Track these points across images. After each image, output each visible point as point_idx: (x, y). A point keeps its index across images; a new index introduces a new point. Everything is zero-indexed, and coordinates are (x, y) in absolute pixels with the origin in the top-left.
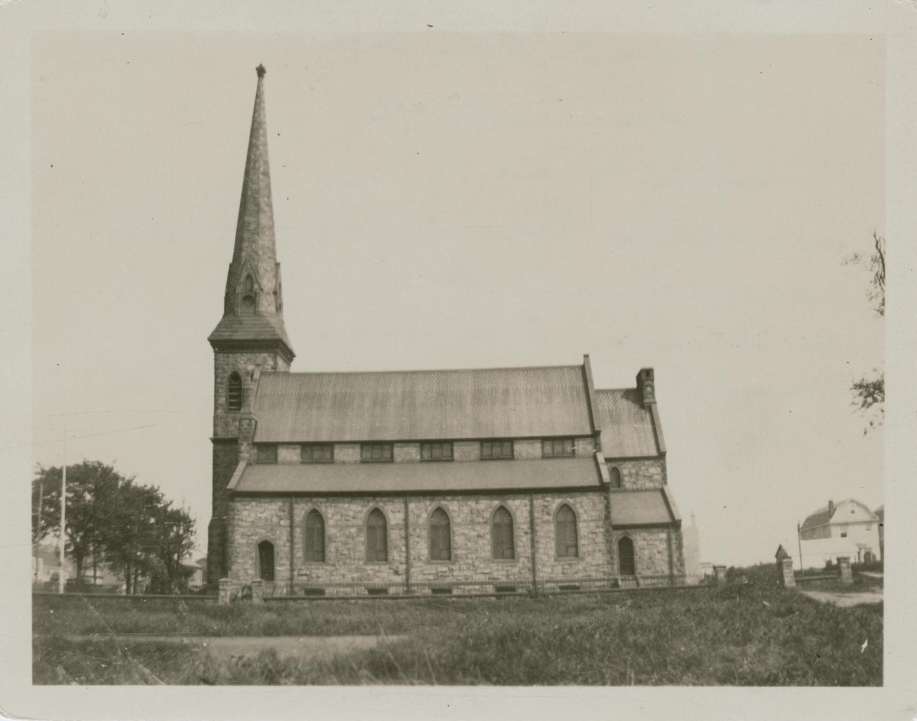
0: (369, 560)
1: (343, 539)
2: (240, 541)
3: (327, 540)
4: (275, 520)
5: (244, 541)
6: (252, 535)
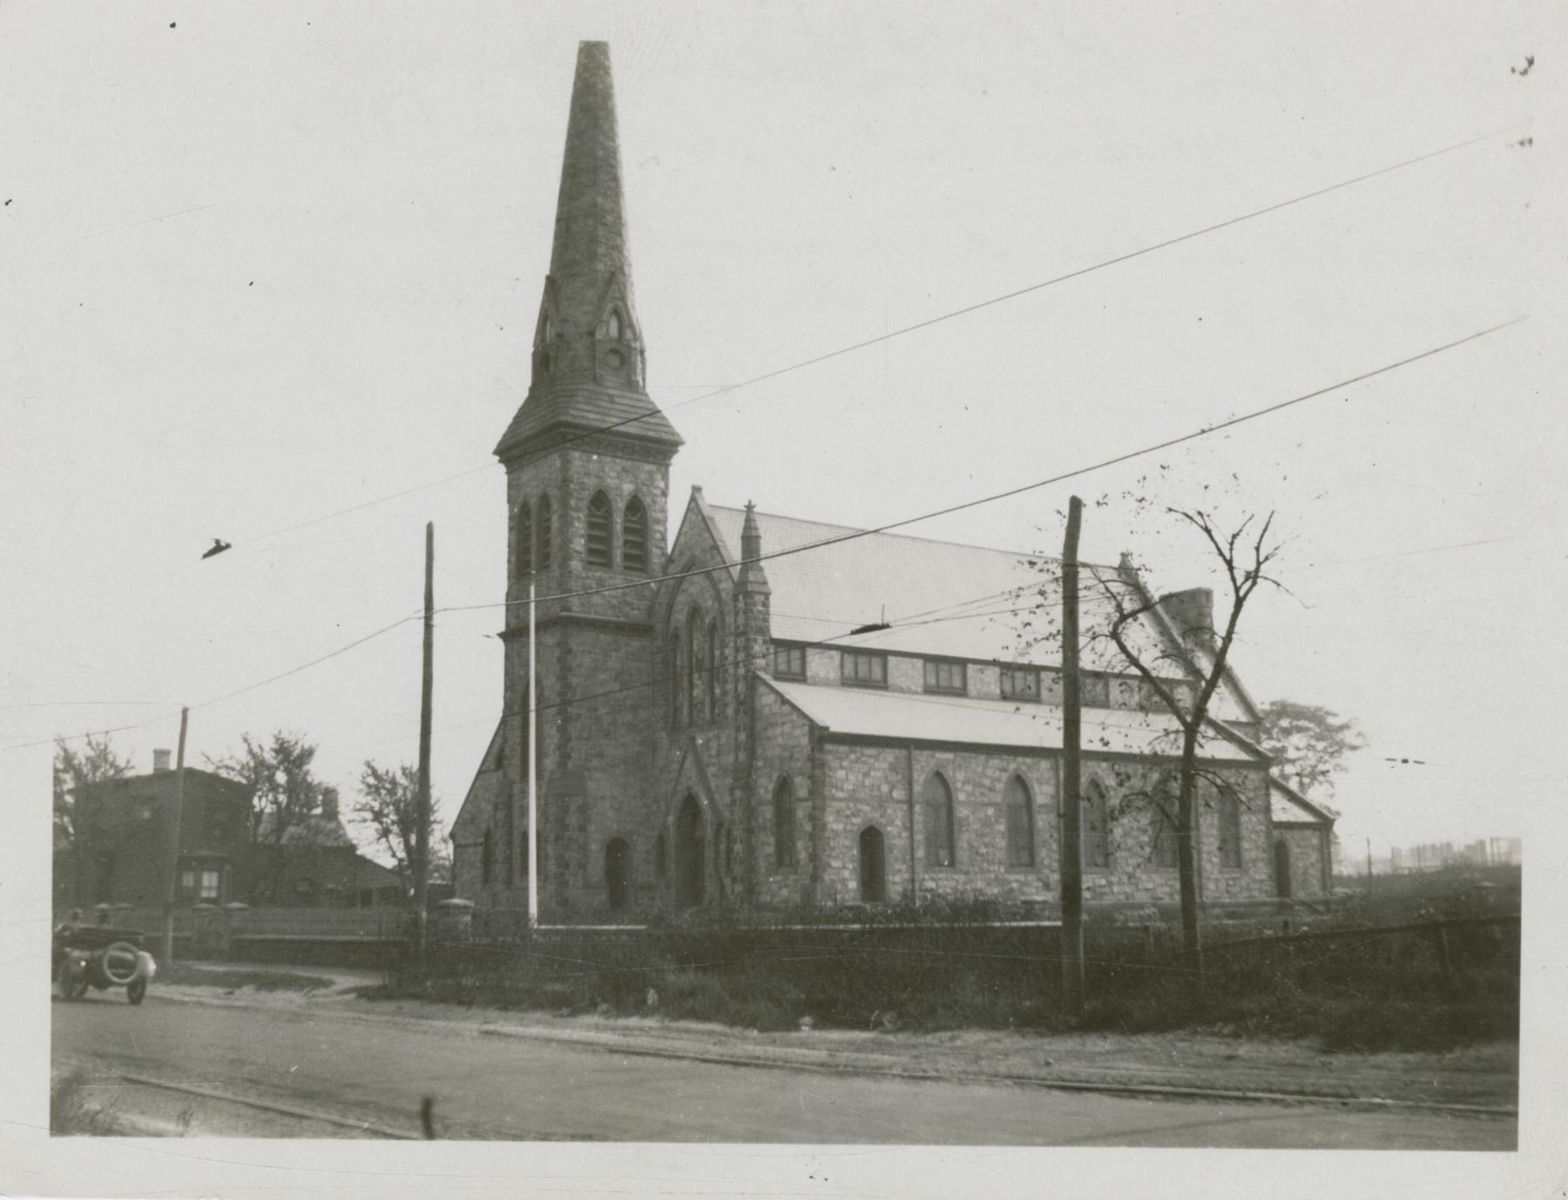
0: (1011, 867)
1: (976, 826)
2: (834, 826)
3: (956, 827)
4: (885, 788)
5: (841, 826)
6: (853, 815)
